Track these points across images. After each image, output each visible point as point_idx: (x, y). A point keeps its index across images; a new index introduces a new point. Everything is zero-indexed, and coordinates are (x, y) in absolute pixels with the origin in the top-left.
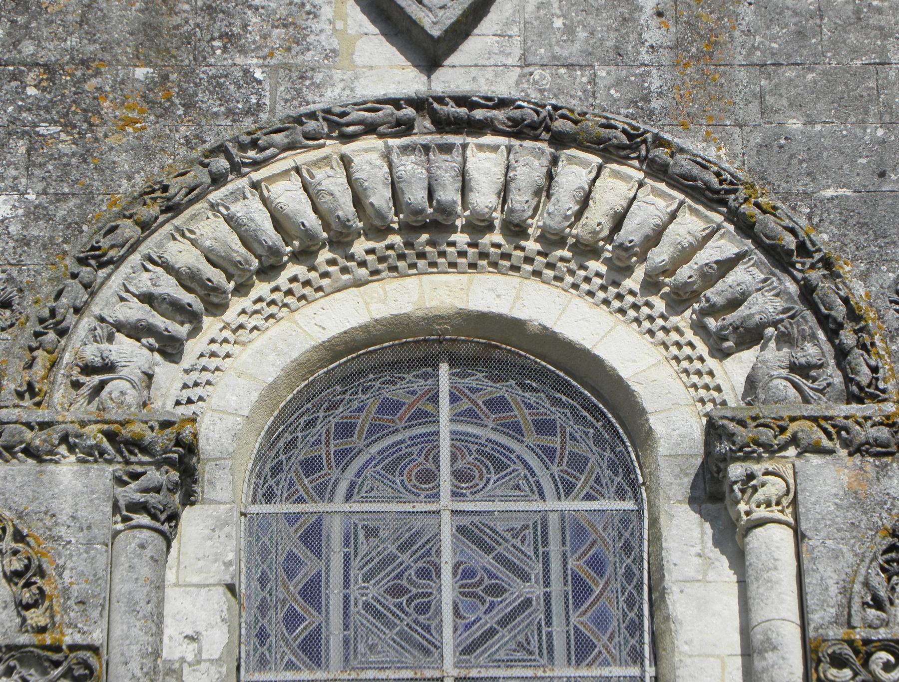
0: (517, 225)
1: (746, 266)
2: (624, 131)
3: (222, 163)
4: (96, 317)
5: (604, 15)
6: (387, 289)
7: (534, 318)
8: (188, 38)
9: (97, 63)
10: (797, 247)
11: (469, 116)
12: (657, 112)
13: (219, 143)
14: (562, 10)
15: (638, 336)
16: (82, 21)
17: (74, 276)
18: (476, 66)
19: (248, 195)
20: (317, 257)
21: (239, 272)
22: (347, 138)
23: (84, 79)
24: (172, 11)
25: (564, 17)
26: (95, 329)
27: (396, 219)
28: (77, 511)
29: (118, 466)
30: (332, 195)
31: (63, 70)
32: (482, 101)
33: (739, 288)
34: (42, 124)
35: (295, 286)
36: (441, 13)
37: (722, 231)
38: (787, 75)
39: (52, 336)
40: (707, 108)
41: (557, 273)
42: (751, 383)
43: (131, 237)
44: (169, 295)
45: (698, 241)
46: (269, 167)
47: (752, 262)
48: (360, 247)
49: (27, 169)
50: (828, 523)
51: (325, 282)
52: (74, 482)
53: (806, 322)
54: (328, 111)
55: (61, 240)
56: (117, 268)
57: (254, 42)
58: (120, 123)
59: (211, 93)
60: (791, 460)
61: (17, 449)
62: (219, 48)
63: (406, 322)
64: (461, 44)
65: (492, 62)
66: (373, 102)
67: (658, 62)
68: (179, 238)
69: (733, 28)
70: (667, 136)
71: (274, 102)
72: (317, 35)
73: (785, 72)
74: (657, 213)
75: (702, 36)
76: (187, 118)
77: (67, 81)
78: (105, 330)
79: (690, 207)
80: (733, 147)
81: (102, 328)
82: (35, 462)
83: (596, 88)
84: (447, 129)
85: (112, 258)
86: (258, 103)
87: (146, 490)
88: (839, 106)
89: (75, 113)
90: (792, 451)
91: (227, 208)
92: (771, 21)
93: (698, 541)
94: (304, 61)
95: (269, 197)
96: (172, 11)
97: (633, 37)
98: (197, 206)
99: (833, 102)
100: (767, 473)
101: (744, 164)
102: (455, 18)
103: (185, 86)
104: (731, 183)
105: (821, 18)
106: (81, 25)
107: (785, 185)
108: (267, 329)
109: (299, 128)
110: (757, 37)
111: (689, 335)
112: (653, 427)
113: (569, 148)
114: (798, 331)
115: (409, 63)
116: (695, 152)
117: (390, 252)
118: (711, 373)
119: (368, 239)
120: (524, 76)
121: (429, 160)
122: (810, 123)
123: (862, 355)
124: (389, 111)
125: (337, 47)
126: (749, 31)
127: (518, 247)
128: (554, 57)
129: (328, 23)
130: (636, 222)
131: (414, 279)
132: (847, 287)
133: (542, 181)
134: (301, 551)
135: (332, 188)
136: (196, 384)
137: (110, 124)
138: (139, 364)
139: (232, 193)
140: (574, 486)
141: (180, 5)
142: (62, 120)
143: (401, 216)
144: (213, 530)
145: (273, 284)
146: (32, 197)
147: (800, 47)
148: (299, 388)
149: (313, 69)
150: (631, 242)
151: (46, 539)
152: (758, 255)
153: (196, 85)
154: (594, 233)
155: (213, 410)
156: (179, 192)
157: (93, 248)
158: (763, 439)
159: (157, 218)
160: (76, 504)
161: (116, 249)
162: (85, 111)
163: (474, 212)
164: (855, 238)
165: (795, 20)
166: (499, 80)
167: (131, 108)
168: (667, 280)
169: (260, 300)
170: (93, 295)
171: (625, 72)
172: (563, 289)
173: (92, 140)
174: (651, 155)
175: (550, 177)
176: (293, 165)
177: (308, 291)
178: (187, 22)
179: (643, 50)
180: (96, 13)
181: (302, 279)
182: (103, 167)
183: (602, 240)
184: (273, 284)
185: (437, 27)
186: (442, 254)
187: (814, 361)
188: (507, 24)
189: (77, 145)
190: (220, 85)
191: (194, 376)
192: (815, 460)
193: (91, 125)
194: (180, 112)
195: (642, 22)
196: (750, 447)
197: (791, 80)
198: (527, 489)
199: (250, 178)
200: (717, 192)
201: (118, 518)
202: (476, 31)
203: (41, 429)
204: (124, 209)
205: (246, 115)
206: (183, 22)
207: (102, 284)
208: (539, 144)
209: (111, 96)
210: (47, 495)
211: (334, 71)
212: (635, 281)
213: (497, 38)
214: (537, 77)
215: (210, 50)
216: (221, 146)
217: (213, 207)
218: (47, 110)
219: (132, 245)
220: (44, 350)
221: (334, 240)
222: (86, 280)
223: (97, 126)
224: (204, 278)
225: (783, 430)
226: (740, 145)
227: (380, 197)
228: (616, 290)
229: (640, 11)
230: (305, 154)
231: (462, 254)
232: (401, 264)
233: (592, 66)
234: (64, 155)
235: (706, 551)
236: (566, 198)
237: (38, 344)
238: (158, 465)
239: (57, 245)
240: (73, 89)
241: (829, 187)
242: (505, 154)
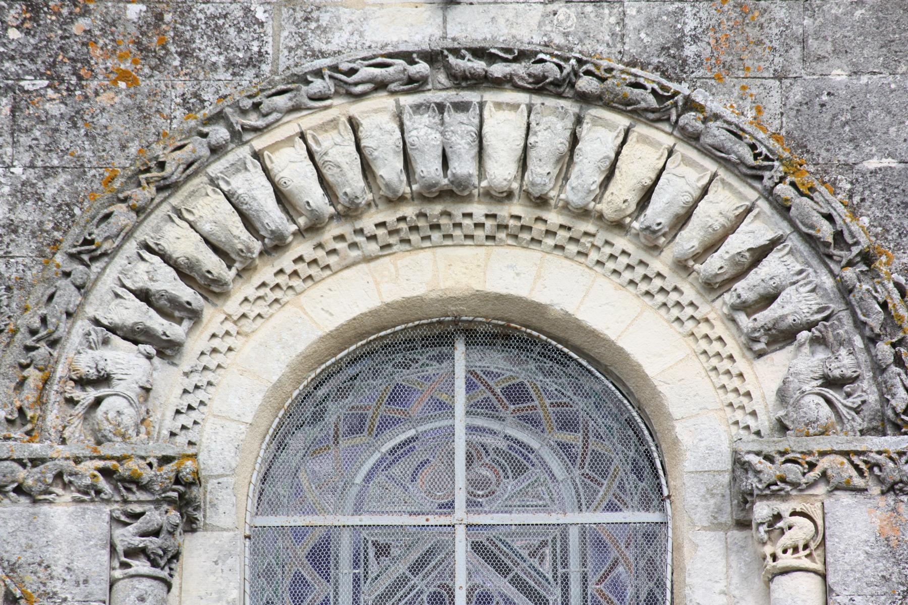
0: (540, 198)
2: (653, 91)
3: (220, 133)
4: (90, 319)
7: (555, 302)
11: (486, 72)
12: (690, 61)
15: (666, 324)
17: (67, 275)
21: (240, 259)
26: (89, 334)
28: (72, 561)
29: (116, 506)
30: (339, 167)
31: (47, 6)
33: (771, 283)
34: (27, 77)
38: (833, 11)
39: (44, 349)
42: (782, 396)
43: (126, 225)
44: (166, 291)
45: (731, 221)
46: (272, 133)
49: (12, 134)
50: (858, 575)
51: (332, 260)
52: (69, 526)
53: (842, 325)
54: (335, 68)
55: (51, 225)
56: (113, 258)
59: (209, 38)
60: (820, 498)
61: (10, 488)
63: (418, 305)
66: (383, 56)
71: (277, 51)
74: (688, 188)
76: (185, 71)
77: (53, 21)
78: (100, 335)
81: (96, 332)
82: (28, 501)
84: (464, 84)
85: (106, 250)
86: (260, 52)
87: (144, 535)
89: (63, 63)
90: (821, 489)
91: (228, 183)
93: (723, 577)
98: (196, 181)
100: (794, 513)
103: (181, 28)
104: (767, 158)
108: (271, 316)
109: (304, 88)
111: (720, 329)
112: (680, 437)
114: (834, 336)
117: (403, 226)
118: (741, 375)
120: (548, 15)
121: (443, 123)
123: (899, 375)
124: (401, 68)
130: (665, 200)
131: (428, 253)
132: (886, 290)
133: (564, 148)
134: (308, 573)
135: (339, 160)
136: (197, 387)
137: (101, 77)
138: (136, 377)
139: (233, 164)
140: (596, 492)
142: (49, 72)
143: (415, 187)
144: (216, 563)
146: (18, 170)
148: (305, 383)
149: (318, 8)
150: (659, 224)
151: (40, 596)
152: (794, 241)
153: (194, 28)
155: (215, 416)
156: (176, 170)
157: (86, 242)
158: (791, 477)
159: (152, 199)
160: (71, 554)
161: (110, 241)
164: (898, 222)
170: (85, 296)
171: (656, 10)
172: (587, 266)
181: (308, 259)
182: (94, 132)
183: (629, 216)
187: (849, 373)
189: (66, 105)
190: (218, 28)
191: (195, 379)
192: (845, 498)
193: (80, 78)
194: (177, 63)
196: (776, 484)
198: (547, 497)
199: (252, 147)
201: (116, 564)
203: (34, 466)
207: (96, 280)
208: (562, 102)
210: (40, 543)
211: (342, 10)
212: (665, 264)
216: (221, 112)
218: (32, 59)
219: (127, 233)
220: (35, 368)
222: (79, 282)
224: (204, 269)
225: (812, 466)
230: (311, 117)
235: (732, 587)
237: (28, 361)
238: (157, 503)
239: (47, 232)
242: (526, 114)
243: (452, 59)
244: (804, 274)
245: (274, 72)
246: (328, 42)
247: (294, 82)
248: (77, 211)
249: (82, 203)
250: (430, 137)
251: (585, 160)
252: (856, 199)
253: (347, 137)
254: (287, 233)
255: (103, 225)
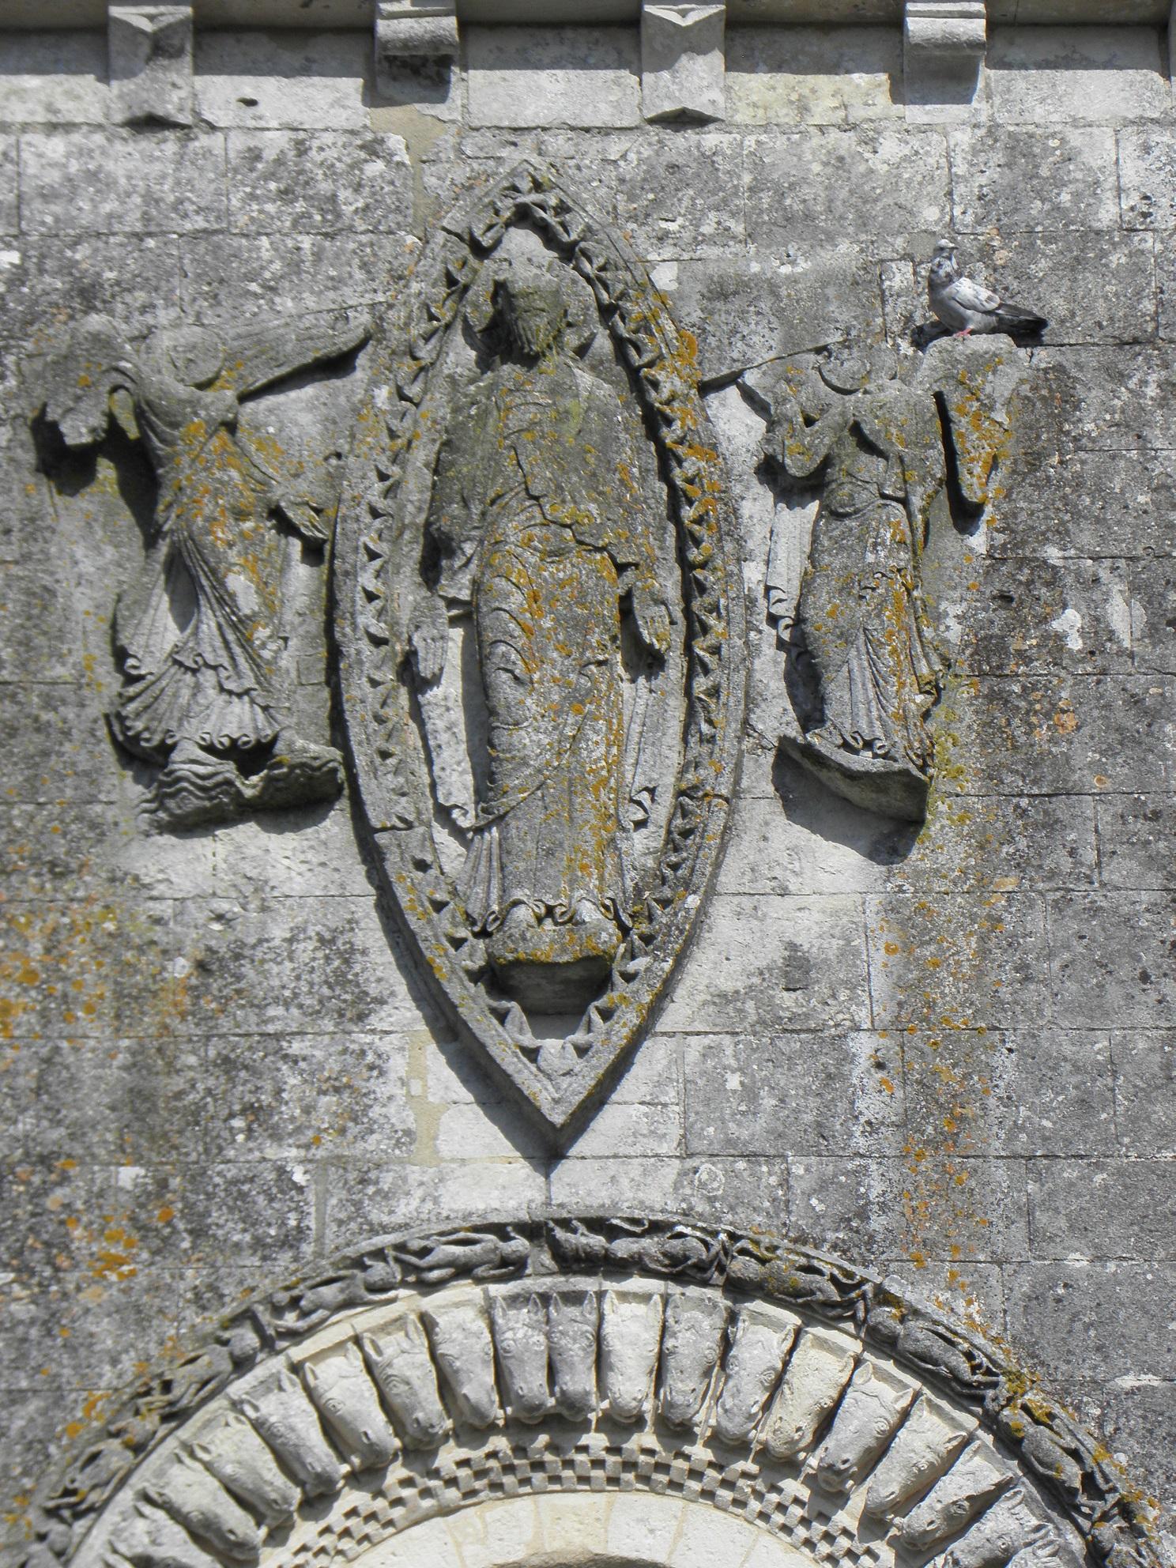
0: (681, 1424)
1: (1009, 1504)
2: (833, 1279)
5: (799, 1068)
6: (488, 1520)
8: (195, 1114)
9: (62, 1160)
10: (1082, 1483)
11: (607, 1250)
13: (244, 1307)
14: (738, 1060)
16: (39, 1088)
17: (42, 1537)
18: (615, 1156)
19: (286, 1384)
20: (384, 1476)
22: (427, 1287)
23: (44, 1191)
24: (172, 1069)
25: (741, 1070)
27: (500, 1413)
30: (408, 1383)
31: (13, 1173)
32: (626, 1226)
35: (352, 1523)
36: (565, 1082)
37: (977, 1443)
38: (1065, 1175)
40: (953, 1232)
41: (738, 1496)
47: (1019, 1497)
48: (448, 1457)
51: (397, 1513)
56: (100, 1515)
57: (293, 1119)
58: (99, 1265)
59: (231, 1210)
62: (241, 1131)
64: (592, 1119)
65: (638, 1149)
67: (878, 1150)
68: (187, 1460)
69: (986, 1091)
70: (894, 1289)
71: (322, 1225)
72: (384, 1106)
73: (1062, 1170)
74: (882, 1411)
75: (941, 1106)
77: (20, 1194)
79: (929, 1401)
80: (989, 1301)
83: (790, 1196)
84: (575, 1267)
88: (1142, 1230)
89: (33, 1249)
91: (256, 1408)
92: (1041, 1080)
94: (365, 1150)
95: (316, 1388)
96: (172, 1069)
97: (842, 1106)
98: (213, 1406)
99: (1132, 1224)
101: (1005, 1330)
102: (586, 1093)
103: (192, 1197)
104: (989, 1372)
105: (1115, 1074)
106: (38, 1095)
107: (1064, 1367)
110: (1022, 1108)
113: (752, 1299)
115: (518, 1154)
116: (936, 1317)
117: (493, 1463)
119: (460, 1445)
121: (548, 1322)
122: (1099, 1258)
124: (490, 1245)
125: (413, 1127)
126: (1009, 1098)
127: (680, 1455)
128: (729, 1142)
129: (399, 1083)
133: (713, 1354)
135: (408, 1373)
139: (262, 1382)
141: (183, 1057)
142: (15, 1262)
145: (322, 1524)
147: (1085, 1126)
149: (378, 1166)
150: (845, 1462)
152: (1027, 1487)
153: (210, 1196)
154: (792, 1442)
157: (67, 1493)
159: (155, 1433)
162: (48, 1245)
163: (614, 1404)
164: (1164, 1461)
165: (1074, 1080)
166: (649, 1180)
167: (114, 1239)
168: (898, 1520)
169: (304, 1548)
173: (59, 1296)
174: (872, 1321)
175: (727, 1343)
176: (351, 1333)
177: (371, 1528)
178: (193, 1086)
179: (857, 1130)
180: (60, 1073)
181: (364, 1512)
182: (75, 1342)
184: (322, 1524)
185: (560, 1109)
186: (569, 1464)
188: (658, 1084)
190: (243, 1196)
194: (186, 1245)
195: (855, 1081)
197: (1072, 1184)
199: (288, 1358)
200: (968, 1385)
202: (614, 1097)
204: (110, 1422)
205: (281, 1247)
206: (187, 1086)
207: (80, 1543)
208: (709, 1292)
209: (85, 1219)
213: (644, 1108)
214: (704, 1177)
215: (226, 1134)
217: (236, 1406)
221: (411, 1447)
223: (65, 1271)
224: (225, 1527)
226: (1000, 1298)
227: (478, 1386)
228: (824, 1528)
229: (852, 1062)
230: (368, 1314)
231: (598, 1464)
232: (509, 1480)
233: (784, 1157)
234: (21, 1322)
236: (750, 1386)
239: (15, 1479)
240: (30, 1207)
241: (1127, 1371)
242: (660, 1308)
243: (560, 1234)
244: (1043, 1532)
245: (319, 1255)
246: (391, 1212)
247: (346, 1268)
248: (53, 1449)
249: (59, 1439)
250: (531, 1341)
251: (742, 1372)
252: (1109, 1429)
253: (418, 1342)
254: (336, 1476)
255: (88, 1470)
